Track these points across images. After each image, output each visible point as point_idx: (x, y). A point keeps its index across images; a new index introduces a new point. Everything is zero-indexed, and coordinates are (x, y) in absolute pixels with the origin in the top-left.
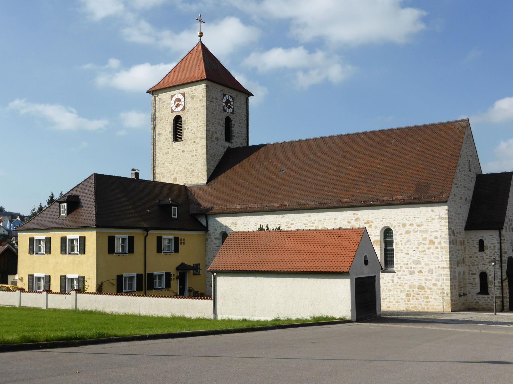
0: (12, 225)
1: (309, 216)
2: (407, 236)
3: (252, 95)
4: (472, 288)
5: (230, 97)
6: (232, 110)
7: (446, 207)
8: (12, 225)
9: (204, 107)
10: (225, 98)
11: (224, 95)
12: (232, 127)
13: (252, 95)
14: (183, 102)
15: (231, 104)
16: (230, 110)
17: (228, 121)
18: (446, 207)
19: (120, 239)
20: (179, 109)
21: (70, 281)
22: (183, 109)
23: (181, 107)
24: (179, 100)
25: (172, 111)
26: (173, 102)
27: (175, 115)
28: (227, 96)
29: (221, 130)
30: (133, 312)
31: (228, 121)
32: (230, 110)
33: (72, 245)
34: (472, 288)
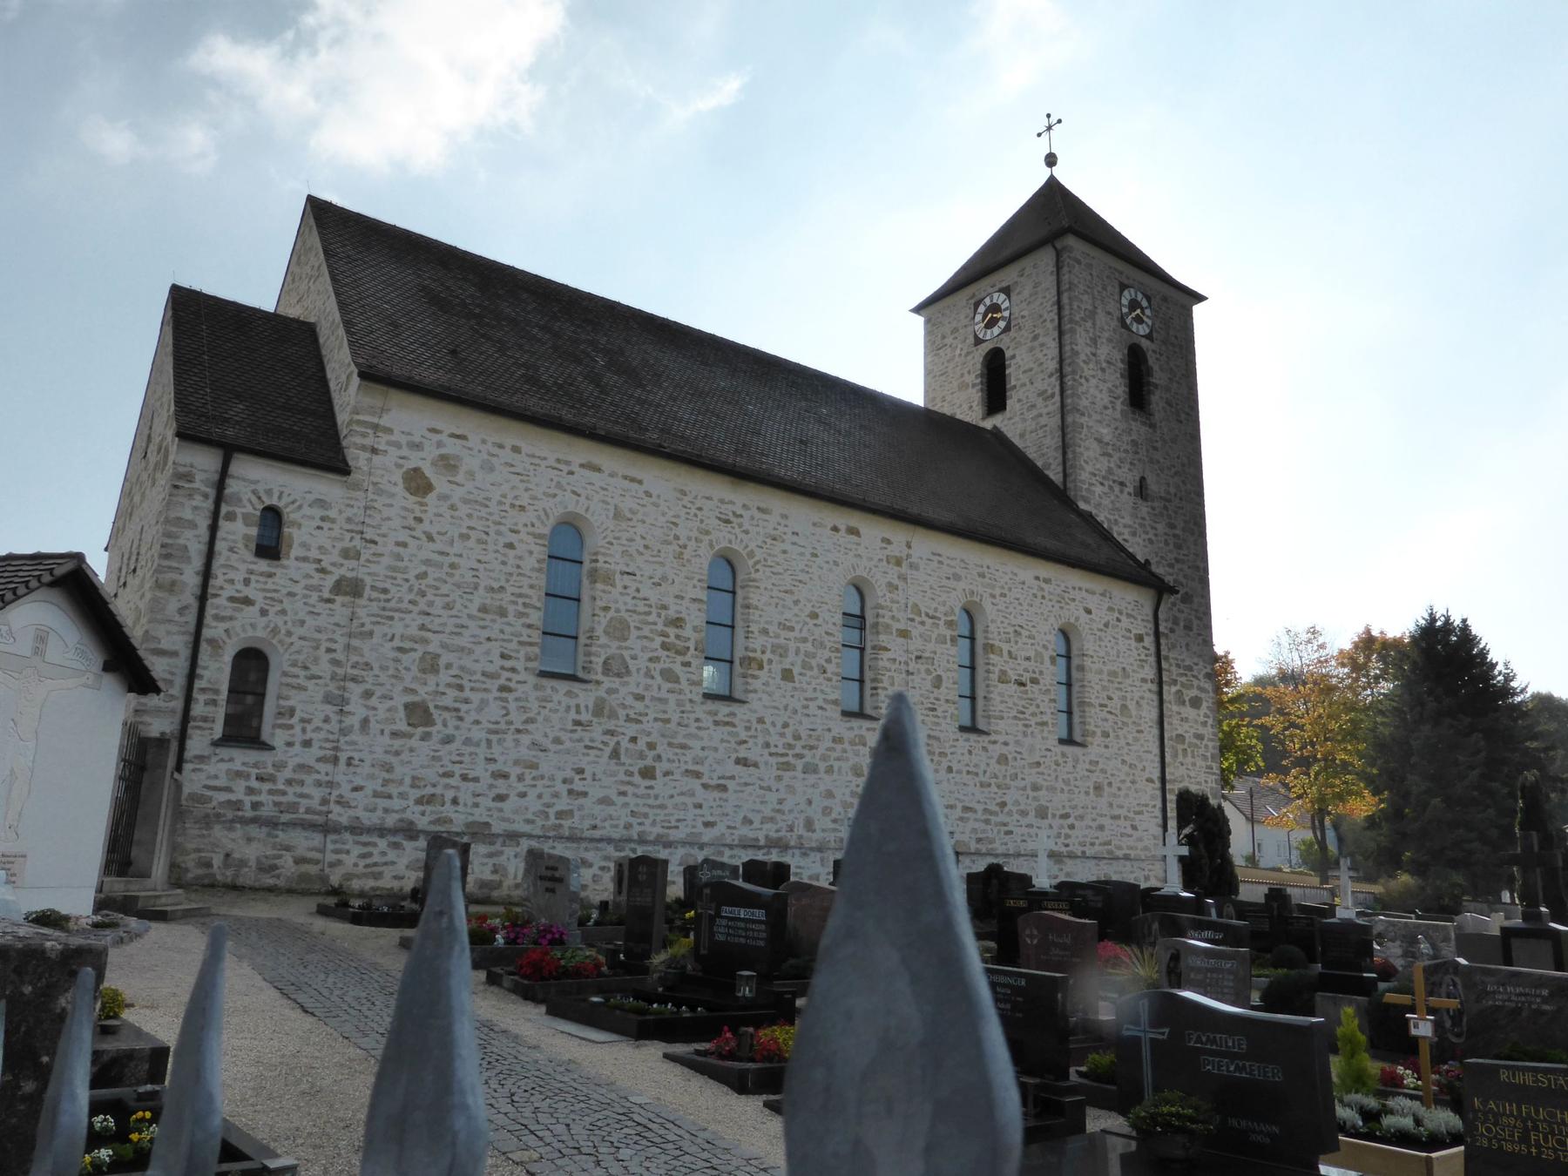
3: (1199, 298)
4: (641, 715)
6: (1148, 331)
7: (1430, 1035)
10: (1126, 293)
11: (1123, 287)
12: (1149, 392)
13: (1199, 298)
14: (1006, 309)
15: (1143, 312)
18: (1430, 1035)
19: (415, 907)
23: (1002, 324)
24: (995, 308)
25: (978, 341)
26: (979, 318)
27: (985, 348)
30: (963, 386)
33: (1553, 925)
34: (641, 715)
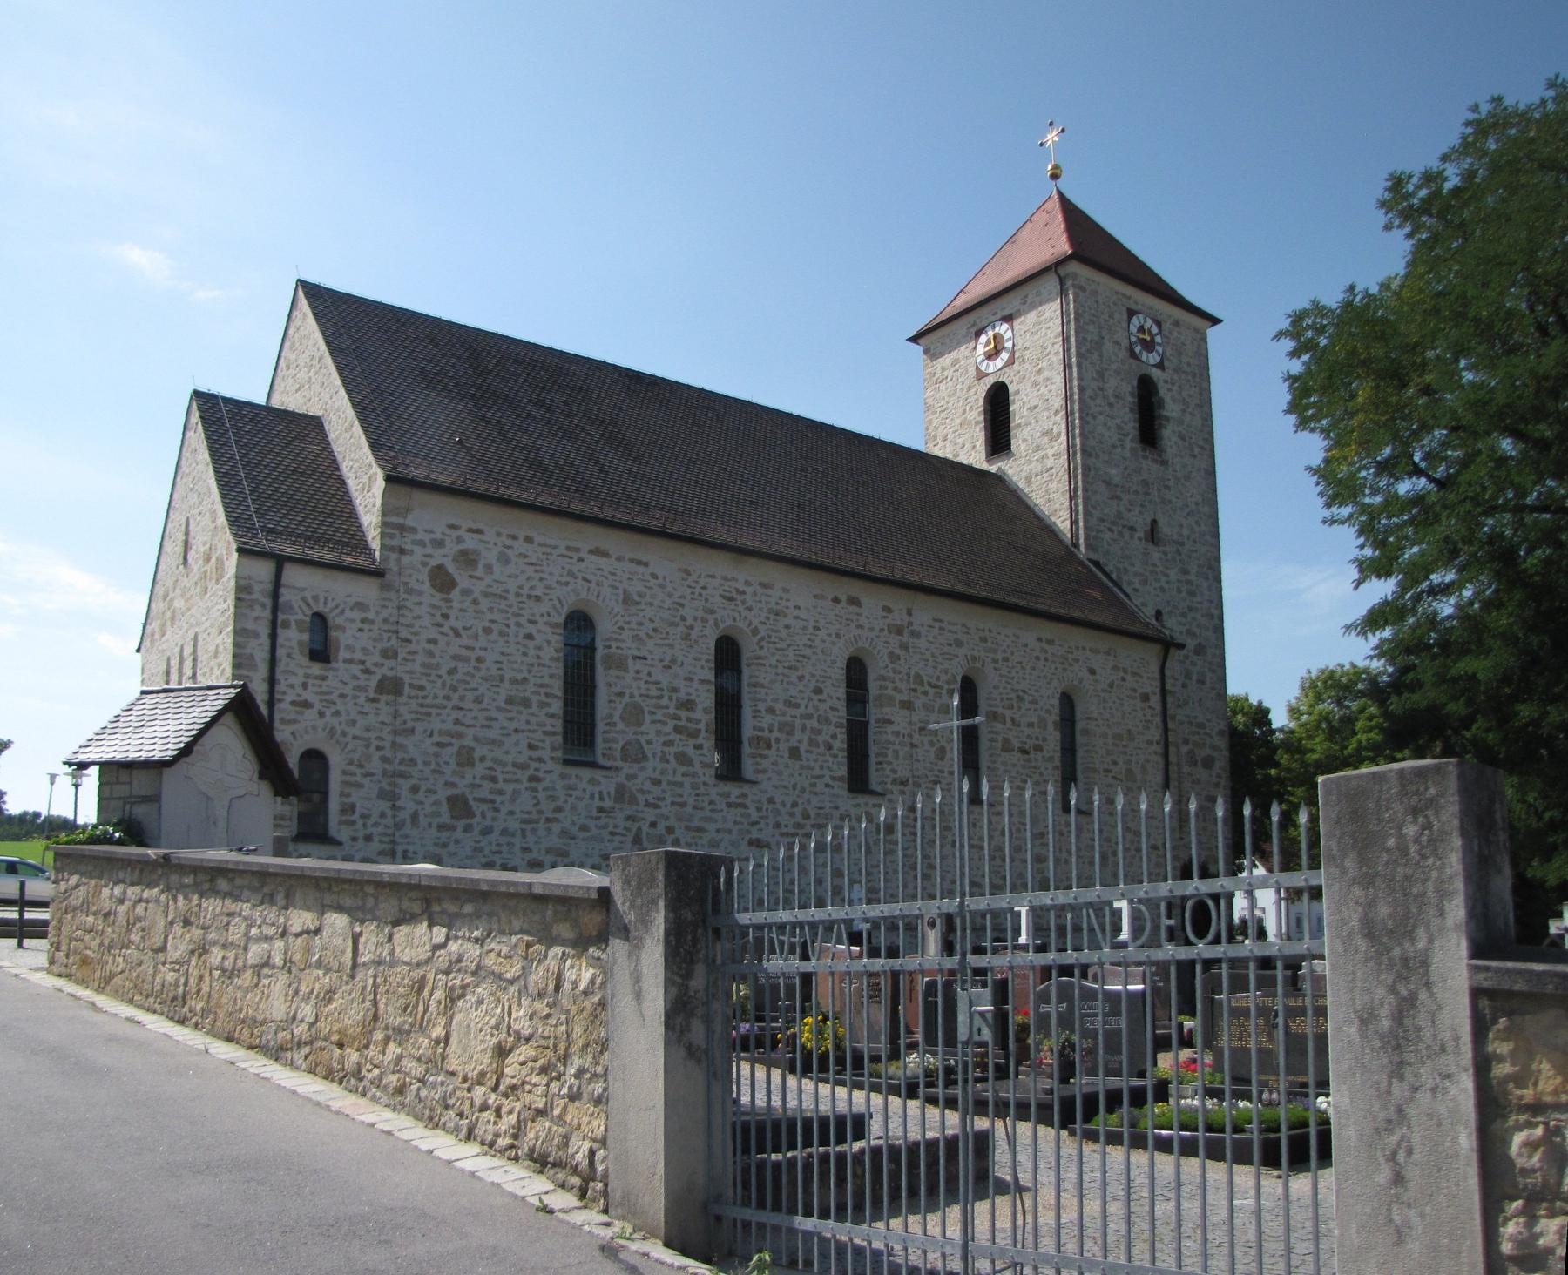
0: (734, 1096)
1: (854, 601)
2: (526, 545)
3: (1215, 321)
5: (1149, 322)
8: (734, 1096)
9: (554, 738)
10: (1135, 320)
11: (1131, 313)
13: (1215, 321)
16: (1153, 358)
17: (1147, 394)
20: (999, 363)
21: (1212, 869)
22: (1010, 362)
25: (980, 375)
27: (988, 382)
28: (1141, 316)
29: (1126, 417)
31: (1147, 394)
32: (1153, 358)
